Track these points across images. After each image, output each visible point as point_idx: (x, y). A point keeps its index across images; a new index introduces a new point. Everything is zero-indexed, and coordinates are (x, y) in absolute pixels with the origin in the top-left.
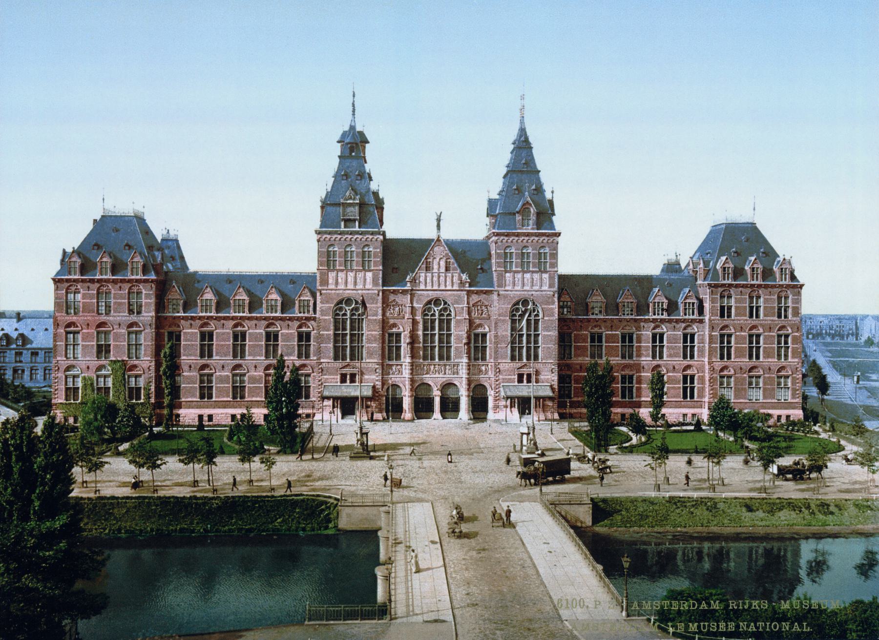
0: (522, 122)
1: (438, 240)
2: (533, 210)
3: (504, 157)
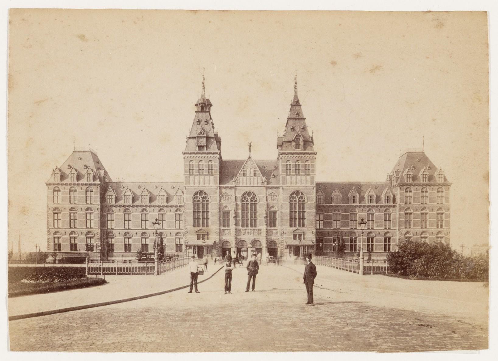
0: (296, 93)
2: (301, 139)
3: (285, 113)
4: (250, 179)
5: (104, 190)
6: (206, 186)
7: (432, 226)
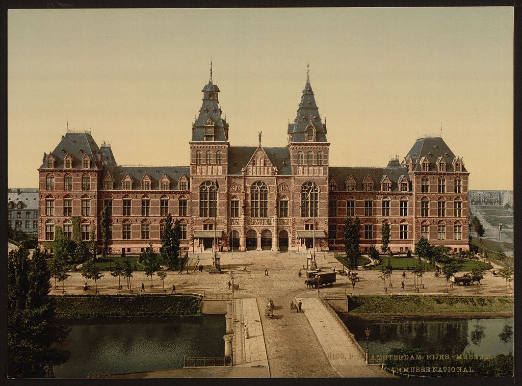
0: (308, 80)
1: (260, 147)
3: (298, 99)
5: (101, 175)
6: (213, 176)
7: (449, 215)
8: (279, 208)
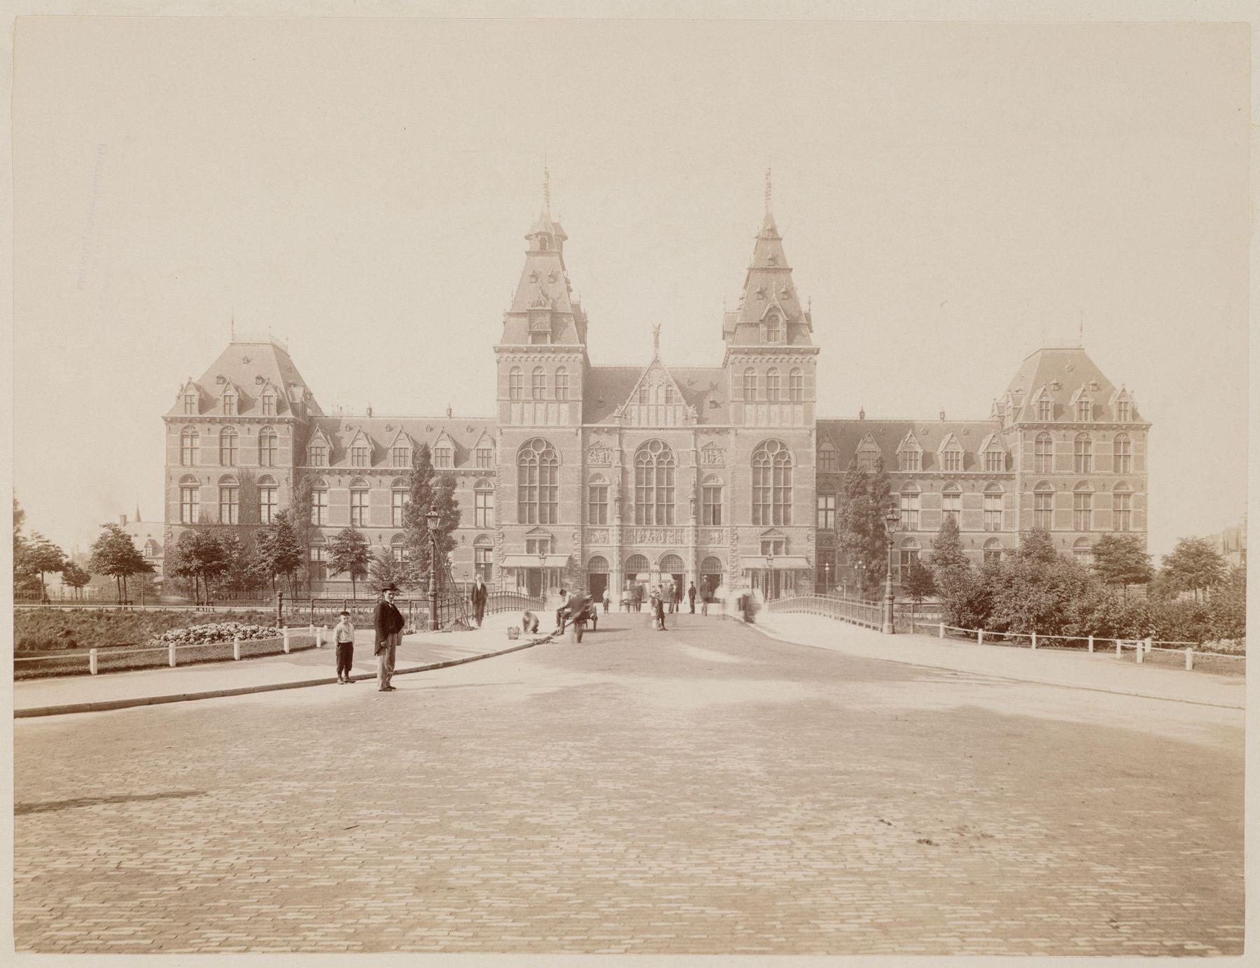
3: (744, 255)
4: (657, 411)
8: (701, 503)
